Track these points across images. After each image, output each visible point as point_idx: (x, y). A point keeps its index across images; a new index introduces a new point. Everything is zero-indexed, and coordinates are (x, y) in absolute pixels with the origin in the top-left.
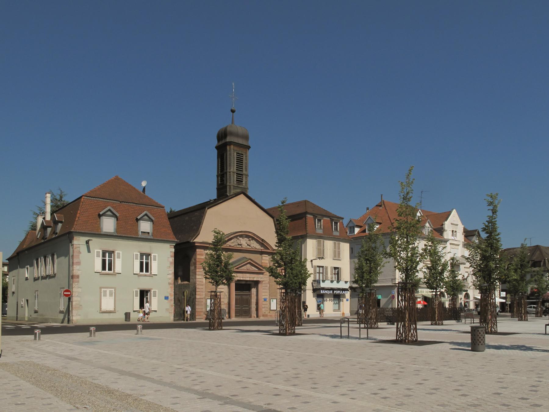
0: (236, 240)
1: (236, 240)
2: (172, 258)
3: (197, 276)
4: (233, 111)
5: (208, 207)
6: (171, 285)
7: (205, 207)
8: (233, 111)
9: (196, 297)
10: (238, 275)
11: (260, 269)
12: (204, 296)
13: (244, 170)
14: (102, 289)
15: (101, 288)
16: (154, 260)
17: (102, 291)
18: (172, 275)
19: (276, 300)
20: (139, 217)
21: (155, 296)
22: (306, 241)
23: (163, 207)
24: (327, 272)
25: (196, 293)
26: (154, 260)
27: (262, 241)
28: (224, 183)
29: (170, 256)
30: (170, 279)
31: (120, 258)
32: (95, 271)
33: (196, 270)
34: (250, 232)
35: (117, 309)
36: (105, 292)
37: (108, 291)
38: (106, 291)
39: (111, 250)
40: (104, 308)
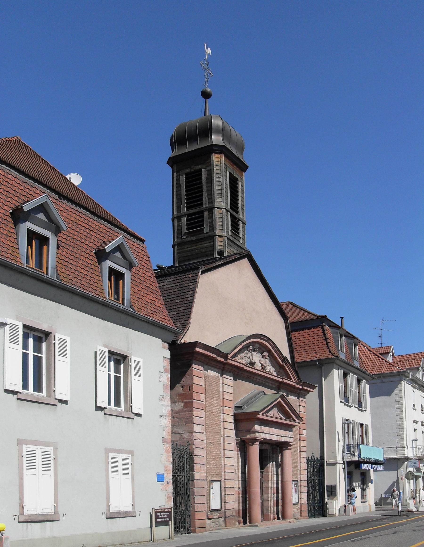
0: (247, 353)
1: (247, 353)
2: (167, 374)
3: (195, 426)
4: (206, 95)
5: (202, 269)
6: (167, 445)
7: (198, 269)
8: (206, 95)
9: (193, 476)
10: (265, 429)
11: (288, 417)
12: (205, 474)
13: (240, 213)
14: (52, 448)
15: (20, 443)
16: (135, 375)
17: (25, 453)
18: (167, 418)
19: (219, 483)
20: (108, 248)
21: (117, 473)
22: (333, 370)
23: (142, 241)
24: (355, 429)
25: (193, 467)
26: (135, 375)
27: (283, 361)
28: (203, 230)
29: (162, 370)
30: (164, 427)
31: (65, 356)
32: (8, 388)
33: (192, 411)
34: (268, 340)
35: (137, 509)
36: (32, 454)
37: (39, 450)
38: (34, 453)
39: (44, 327)
40: (213, 507)
